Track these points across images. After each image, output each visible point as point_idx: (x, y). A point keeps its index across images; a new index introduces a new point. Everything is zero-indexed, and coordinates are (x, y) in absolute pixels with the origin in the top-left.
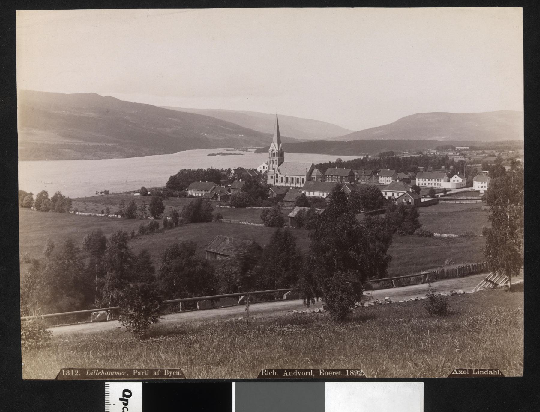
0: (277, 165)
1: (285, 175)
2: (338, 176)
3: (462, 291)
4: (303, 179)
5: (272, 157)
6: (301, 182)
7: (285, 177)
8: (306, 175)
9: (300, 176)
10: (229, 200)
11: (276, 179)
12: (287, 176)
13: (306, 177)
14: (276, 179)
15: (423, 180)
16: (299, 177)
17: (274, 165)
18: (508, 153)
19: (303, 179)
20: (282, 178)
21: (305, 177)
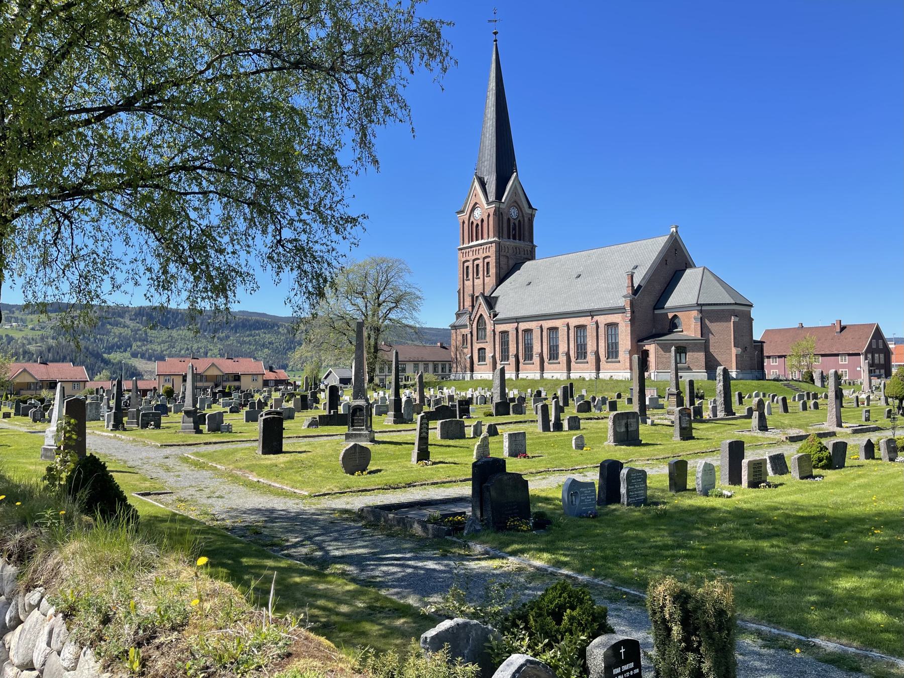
5: (471, 244)
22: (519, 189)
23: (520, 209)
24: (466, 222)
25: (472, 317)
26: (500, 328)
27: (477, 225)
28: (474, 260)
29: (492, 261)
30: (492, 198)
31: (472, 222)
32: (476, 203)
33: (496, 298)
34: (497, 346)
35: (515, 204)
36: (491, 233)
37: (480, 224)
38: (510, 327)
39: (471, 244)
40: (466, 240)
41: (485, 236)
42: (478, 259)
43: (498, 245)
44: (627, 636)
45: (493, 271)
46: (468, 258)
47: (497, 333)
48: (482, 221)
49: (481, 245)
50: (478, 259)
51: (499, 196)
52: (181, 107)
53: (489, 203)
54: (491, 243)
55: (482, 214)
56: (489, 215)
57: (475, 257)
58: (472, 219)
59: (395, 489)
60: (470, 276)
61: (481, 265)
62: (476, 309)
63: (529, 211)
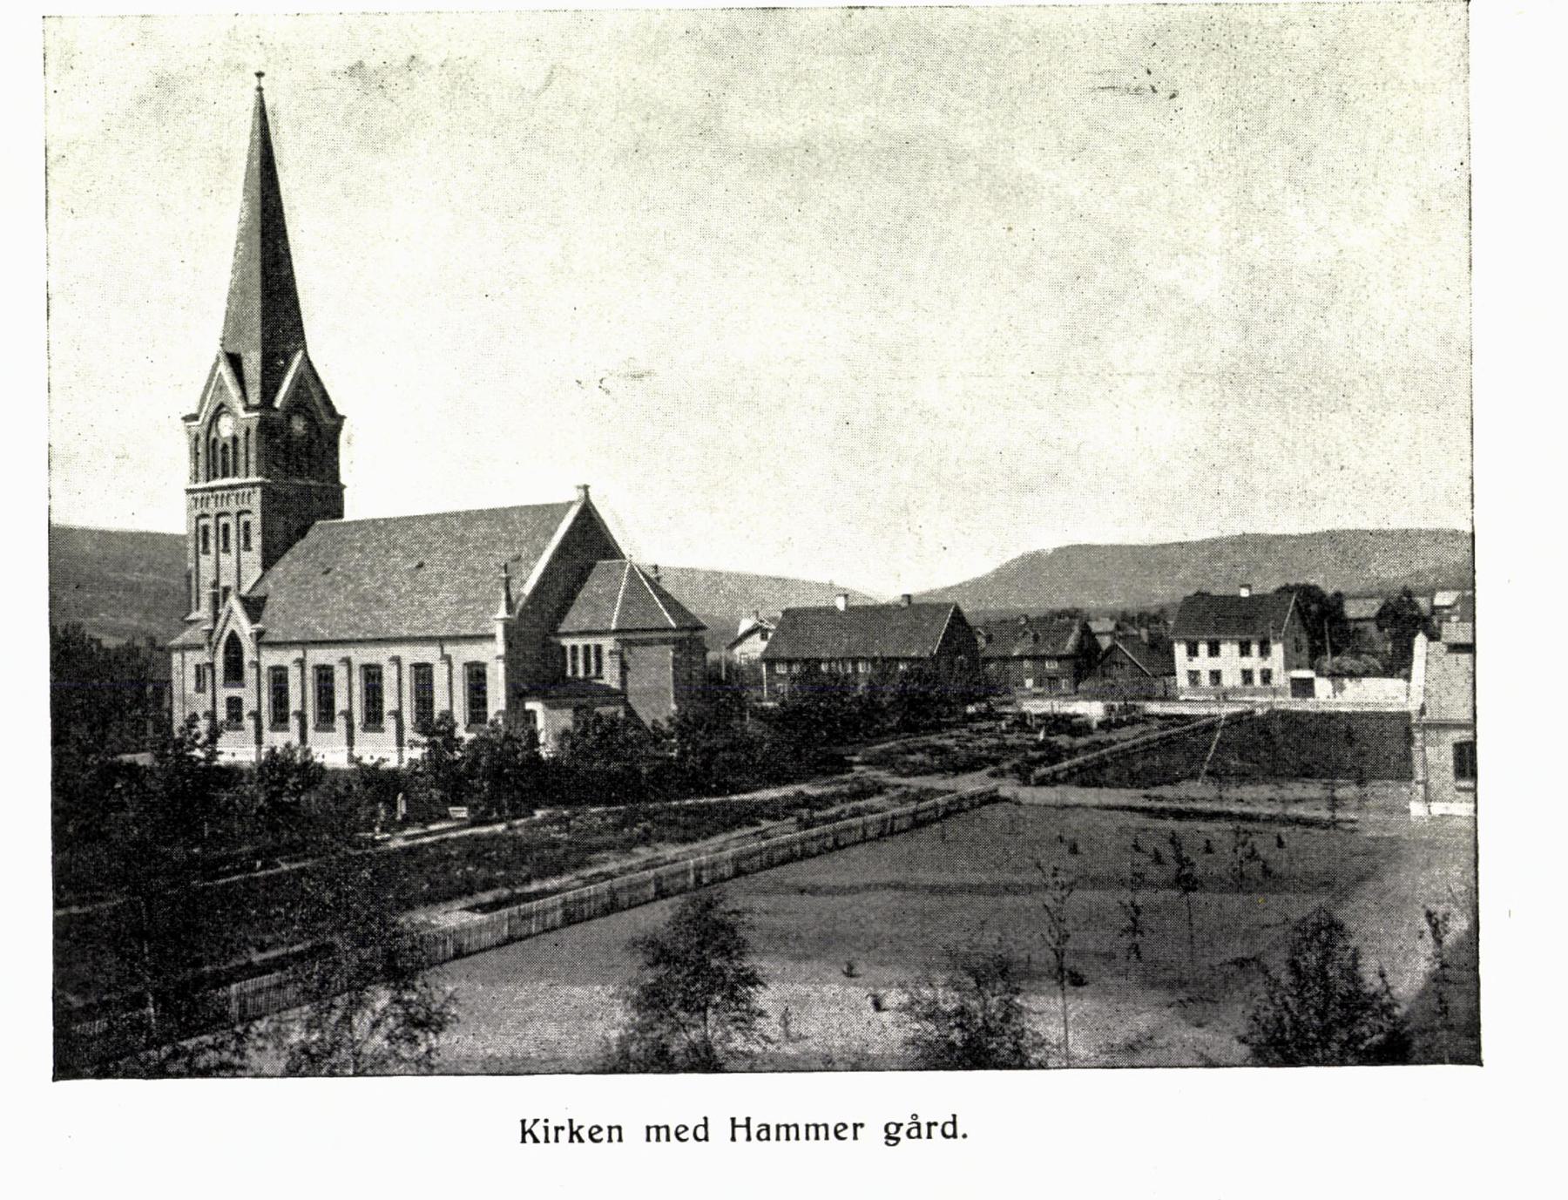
0: (253, 559)
1: (304, 644)
2: (855, 661)
3: (1457, 928)
4: (477, 675)
5: (213, 483)
6: (358, 718)
7: (301, 663)
8: (499, 630)
9: (441, 641)
10: (348, 1067)
11: (224, 693)
12: (318, 656)
13: (500, 647)
14: (224, 693)
15: (1245, 651)
16: (429, 654)
17: (228, 561)
18: (1096, 955)
19: (477, 675)
20: (279, 678)
21: (492, 654)
22: (309, 376)
23: (311, 420)
24: (202, 439)
25: (214, 639)
26: (271, 658)
27: (225, 447)
28: (219, 515)
29: (256, 520)
30: (255, 399)
31: (215, 441)
32: (222, 405)
33: (263, 599)
34: (265, 695)
35: (298, 404)
36: (252, 467)
37: (230, 443)
38: (287, 658)
39: (213, 483)
40: (202, 473)
41: (242, 472)
42: (226, 514)
43: (269, 495)
44: (537, 557)
45: (256, 541)
46: (225, 508)
47: (264, 670)
48: (235, 439)
49: (231, 487)
50: (226, 514)
51: (269, 391)
52: (506, 868)
53: (247, 409)
54: (253, 485)
55: (237, 426)
56: (248, 432)
57: (220, 509)
58: (213, 435)
59: (1474, 572)
60: (212, 548)
61: (233, 528)
62: (221, 621)
63: (327, 421)
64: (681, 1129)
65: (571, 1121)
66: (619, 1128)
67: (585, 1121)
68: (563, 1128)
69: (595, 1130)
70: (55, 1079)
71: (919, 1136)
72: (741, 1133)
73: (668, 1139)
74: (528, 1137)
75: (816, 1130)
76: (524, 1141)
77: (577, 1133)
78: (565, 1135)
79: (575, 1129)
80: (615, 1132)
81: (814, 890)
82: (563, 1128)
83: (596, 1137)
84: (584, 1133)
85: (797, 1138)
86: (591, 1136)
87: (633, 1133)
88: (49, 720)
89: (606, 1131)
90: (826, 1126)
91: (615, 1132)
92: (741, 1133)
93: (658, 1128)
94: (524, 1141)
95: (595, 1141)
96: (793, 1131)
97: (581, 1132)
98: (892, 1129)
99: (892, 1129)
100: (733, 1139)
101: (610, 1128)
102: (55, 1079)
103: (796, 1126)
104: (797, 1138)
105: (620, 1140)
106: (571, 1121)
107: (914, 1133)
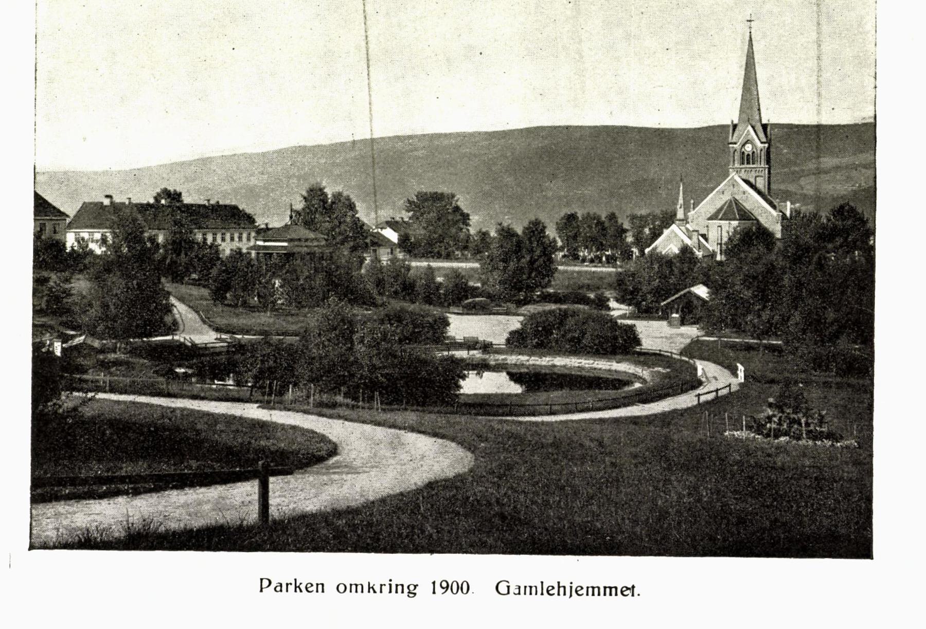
30: (764, 140)
64: (579, 589)
65: (295, 580)
66: (323, 585)
67: (303, 581)
68: (291, 584)
69: (309, 585)
70: (872, 559)
71: (281, 591)
72: (439, 590)
73: (616, 595)
74: (371, 590)
75: (610, 590)
76: (296, 591)
77: (299, 587)
78: (292, 588)
79: (298, 585)
80: (320, 587)
81: (708, 393)
82: (291, 584)
83: (550, 592)
84: (303, 587)
85: (599, 595)
86: (306, 588)
87: (330, 588)
88: (30, 467)
89: (315, 586)
90: (616, 588)
91: (320, 587)
92: (439, 590)
93: (593, 588)
94: (296, 591)
95: (549, 594)
96: (596, 590)
97: (301, 586)
98: (412, 588)
99: (412, 588)
100: (434, 593)
101: (317, 585)
102: (872, 559)
103: (599, 588)
104: (599, 595)
105: (323, 591)
106: (295, 580)
107: (278, 589)
